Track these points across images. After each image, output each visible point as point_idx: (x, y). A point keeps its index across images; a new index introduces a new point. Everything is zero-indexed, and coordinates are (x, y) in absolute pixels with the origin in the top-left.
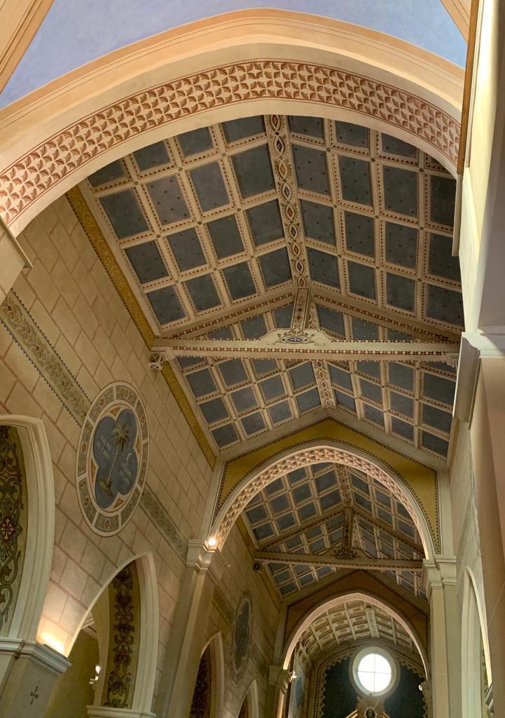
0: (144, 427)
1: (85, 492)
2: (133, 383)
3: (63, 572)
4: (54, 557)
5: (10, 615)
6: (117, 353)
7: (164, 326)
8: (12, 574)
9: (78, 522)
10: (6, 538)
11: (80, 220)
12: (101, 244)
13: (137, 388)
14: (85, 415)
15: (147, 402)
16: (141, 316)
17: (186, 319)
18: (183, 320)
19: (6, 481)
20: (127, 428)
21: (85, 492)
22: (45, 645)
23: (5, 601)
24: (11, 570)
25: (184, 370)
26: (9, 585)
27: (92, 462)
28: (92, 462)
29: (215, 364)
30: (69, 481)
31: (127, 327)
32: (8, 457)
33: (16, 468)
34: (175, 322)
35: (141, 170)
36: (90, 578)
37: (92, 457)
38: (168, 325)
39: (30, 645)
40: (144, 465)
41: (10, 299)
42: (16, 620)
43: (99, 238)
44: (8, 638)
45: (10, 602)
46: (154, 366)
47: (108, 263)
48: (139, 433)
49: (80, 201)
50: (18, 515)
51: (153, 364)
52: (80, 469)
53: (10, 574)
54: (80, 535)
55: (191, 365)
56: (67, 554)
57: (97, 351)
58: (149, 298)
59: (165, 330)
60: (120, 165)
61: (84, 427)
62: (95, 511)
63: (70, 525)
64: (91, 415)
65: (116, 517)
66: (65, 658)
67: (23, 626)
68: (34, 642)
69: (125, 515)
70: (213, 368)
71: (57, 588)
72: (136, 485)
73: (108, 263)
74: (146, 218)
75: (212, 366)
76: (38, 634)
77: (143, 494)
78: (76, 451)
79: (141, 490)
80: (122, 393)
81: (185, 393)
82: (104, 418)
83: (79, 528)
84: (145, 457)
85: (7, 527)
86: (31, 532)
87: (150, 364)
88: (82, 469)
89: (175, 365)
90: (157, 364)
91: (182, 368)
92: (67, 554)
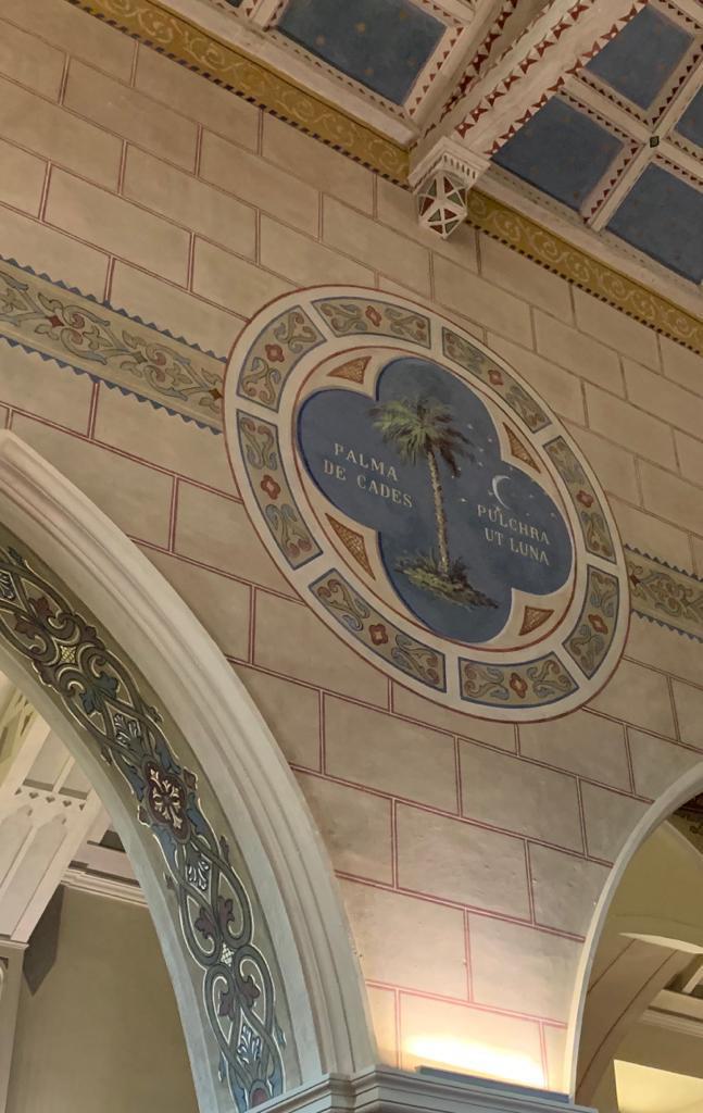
0: (517, 396)
1: (356, 613)
2: (386, 284)
3: (394, 846)
4: (313, 802)
5: (282, 1022)
6: (259, 213)
7: (410, 103)
8: (238, 911)
9: (376, 693)
10: (178, 822)
11: (660, 331)
12: (672, 321)
13: (417, 299)
14: (217, 395)
15: (485, 330)
16: (617, 283)
17: (450, 33)
18: (443, 44)
19: (80, 670)
20: (437, 409)
21: (356, 613)
22: (424, 1070)
23: (257, 994)
24: (230, 901)
25: (586, 212)
26: (247, 945)
27: (330, 519)
28: (330, 519)
29: (661, 133)
30: (254, 588)
31: (260, 136)
32: (31, 600)
33: (67, 617)
34: (430, 67)
35: (645, 106)
36: (537, 849)
37: (323, 505)
38: (417, 91)
39: (365, 1083)
40: (584, 499)
41: (645, 598)
42: (302, 1026)
43: (528, 229)
44: (304, 1087)
45: (269, 989)
46: (437, 216)
47: (649, 313)
48: (500, 415)
49: (159, 19)
50: (162, 747)
51: (432, 211)
52: (289, 550)
53: (235, 912)
54: (408, 732)
55: (595, 184)
56: (386, 796)
57: (160, 216)
58: (291, 37)
59: (418, 108)
60: (557, 100)
61: (232, 430)
62: (436, 657)
63: (339, 713)
64: (245, 390)
65: (272, 403)
66: (563, 1098)
67: (327, 1044)
68: (368, 1070)
69: (590, 643)
70: (664, 148)
71: (393, 898)
72: (583, 558)
73: (649, 313)
74: (580, 110)
75: (654, 142)
76: (379, 1045)
77: (633, 579)
78: (241, 501)
79: (619, 570)
80: (349, 318)
81: (638, 279)
82: (313, 396)
83: (389, 711)
84: (571, 474)
85: (164, 793)
86: (213, 768)
87: (424, 222)
88: (299, 547)
89: (539, 209)
90: (441, 203)
91: (577, 210)
92: (386, 796)
